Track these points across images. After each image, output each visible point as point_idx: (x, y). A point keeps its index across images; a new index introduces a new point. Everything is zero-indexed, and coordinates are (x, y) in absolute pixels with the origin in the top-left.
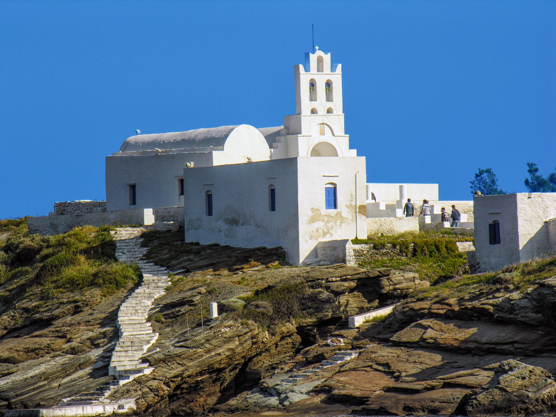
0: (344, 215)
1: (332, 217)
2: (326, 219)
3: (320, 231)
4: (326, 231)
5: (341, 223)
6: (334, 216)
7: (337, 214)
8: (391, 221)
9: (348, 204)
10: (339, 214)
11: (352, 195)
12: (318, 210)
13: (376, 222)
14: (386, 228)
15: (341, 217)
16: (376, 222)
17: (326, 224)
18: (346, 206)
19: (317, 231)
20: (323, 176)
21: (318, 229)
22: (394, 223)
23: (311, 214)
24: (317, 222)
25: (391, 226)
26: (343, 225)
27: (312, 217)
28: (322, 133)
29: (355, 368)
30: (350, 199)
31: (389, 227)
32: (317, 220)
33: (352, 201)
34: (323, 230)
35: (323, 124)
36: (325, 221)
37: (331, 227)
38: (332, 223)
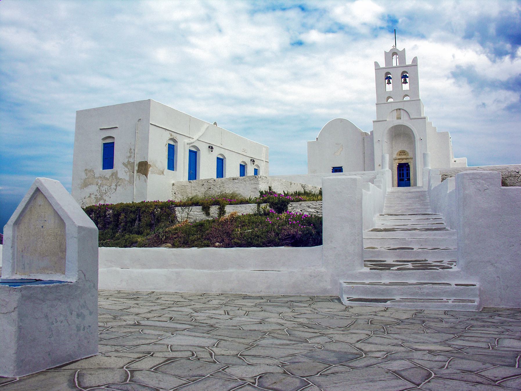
0: (120, 175)
1: (107, 179)
2: (100, 182)
3: (93, 196)
4: (99, 197)
5: (116, 186)
6: (108, 177)
7: (112, 175)
8: (222, 183)
9: (126, 161)
10: (115, 175)
11: (131, 149)
12: (91, 171)
13: (203, 185)
14: (216, 192)
15: (117, 178)
16: (203, 185)
17: (99, 188)
18: (124, 164)
19: (89, 197)
20: (100, 129)
21: (90, 194)
22: (226, 186)
23: (84, 176)
24: (90, 186)
25: (222, 189)
26: (119, 188)
27: (85, 180)
28: (399, 118)
29: (29, 378)
30: (129, 154)
31: (219, 191)
32: (91, 184)
33: (130, 157)
34: (96, 195)
35: (400, 109)
36: (99, 184)
37: (104, 192)
38: (106, 187)
